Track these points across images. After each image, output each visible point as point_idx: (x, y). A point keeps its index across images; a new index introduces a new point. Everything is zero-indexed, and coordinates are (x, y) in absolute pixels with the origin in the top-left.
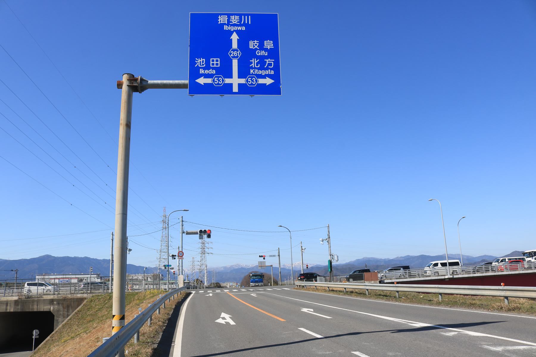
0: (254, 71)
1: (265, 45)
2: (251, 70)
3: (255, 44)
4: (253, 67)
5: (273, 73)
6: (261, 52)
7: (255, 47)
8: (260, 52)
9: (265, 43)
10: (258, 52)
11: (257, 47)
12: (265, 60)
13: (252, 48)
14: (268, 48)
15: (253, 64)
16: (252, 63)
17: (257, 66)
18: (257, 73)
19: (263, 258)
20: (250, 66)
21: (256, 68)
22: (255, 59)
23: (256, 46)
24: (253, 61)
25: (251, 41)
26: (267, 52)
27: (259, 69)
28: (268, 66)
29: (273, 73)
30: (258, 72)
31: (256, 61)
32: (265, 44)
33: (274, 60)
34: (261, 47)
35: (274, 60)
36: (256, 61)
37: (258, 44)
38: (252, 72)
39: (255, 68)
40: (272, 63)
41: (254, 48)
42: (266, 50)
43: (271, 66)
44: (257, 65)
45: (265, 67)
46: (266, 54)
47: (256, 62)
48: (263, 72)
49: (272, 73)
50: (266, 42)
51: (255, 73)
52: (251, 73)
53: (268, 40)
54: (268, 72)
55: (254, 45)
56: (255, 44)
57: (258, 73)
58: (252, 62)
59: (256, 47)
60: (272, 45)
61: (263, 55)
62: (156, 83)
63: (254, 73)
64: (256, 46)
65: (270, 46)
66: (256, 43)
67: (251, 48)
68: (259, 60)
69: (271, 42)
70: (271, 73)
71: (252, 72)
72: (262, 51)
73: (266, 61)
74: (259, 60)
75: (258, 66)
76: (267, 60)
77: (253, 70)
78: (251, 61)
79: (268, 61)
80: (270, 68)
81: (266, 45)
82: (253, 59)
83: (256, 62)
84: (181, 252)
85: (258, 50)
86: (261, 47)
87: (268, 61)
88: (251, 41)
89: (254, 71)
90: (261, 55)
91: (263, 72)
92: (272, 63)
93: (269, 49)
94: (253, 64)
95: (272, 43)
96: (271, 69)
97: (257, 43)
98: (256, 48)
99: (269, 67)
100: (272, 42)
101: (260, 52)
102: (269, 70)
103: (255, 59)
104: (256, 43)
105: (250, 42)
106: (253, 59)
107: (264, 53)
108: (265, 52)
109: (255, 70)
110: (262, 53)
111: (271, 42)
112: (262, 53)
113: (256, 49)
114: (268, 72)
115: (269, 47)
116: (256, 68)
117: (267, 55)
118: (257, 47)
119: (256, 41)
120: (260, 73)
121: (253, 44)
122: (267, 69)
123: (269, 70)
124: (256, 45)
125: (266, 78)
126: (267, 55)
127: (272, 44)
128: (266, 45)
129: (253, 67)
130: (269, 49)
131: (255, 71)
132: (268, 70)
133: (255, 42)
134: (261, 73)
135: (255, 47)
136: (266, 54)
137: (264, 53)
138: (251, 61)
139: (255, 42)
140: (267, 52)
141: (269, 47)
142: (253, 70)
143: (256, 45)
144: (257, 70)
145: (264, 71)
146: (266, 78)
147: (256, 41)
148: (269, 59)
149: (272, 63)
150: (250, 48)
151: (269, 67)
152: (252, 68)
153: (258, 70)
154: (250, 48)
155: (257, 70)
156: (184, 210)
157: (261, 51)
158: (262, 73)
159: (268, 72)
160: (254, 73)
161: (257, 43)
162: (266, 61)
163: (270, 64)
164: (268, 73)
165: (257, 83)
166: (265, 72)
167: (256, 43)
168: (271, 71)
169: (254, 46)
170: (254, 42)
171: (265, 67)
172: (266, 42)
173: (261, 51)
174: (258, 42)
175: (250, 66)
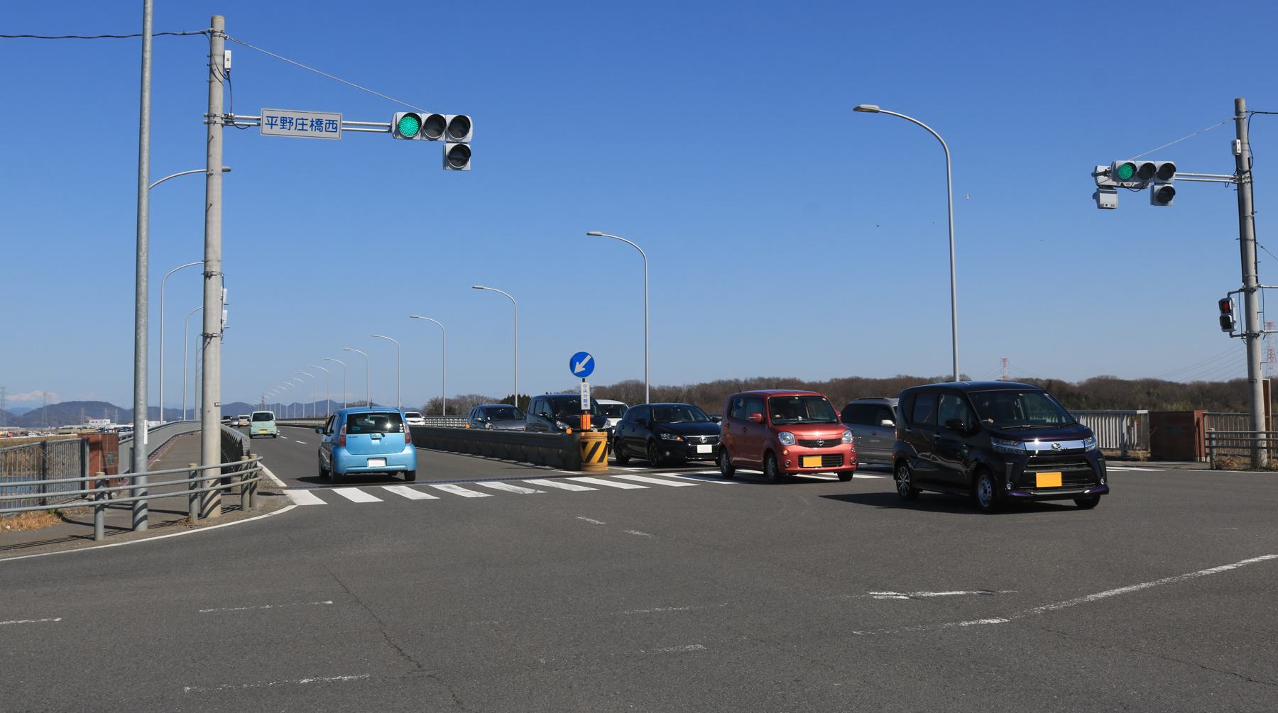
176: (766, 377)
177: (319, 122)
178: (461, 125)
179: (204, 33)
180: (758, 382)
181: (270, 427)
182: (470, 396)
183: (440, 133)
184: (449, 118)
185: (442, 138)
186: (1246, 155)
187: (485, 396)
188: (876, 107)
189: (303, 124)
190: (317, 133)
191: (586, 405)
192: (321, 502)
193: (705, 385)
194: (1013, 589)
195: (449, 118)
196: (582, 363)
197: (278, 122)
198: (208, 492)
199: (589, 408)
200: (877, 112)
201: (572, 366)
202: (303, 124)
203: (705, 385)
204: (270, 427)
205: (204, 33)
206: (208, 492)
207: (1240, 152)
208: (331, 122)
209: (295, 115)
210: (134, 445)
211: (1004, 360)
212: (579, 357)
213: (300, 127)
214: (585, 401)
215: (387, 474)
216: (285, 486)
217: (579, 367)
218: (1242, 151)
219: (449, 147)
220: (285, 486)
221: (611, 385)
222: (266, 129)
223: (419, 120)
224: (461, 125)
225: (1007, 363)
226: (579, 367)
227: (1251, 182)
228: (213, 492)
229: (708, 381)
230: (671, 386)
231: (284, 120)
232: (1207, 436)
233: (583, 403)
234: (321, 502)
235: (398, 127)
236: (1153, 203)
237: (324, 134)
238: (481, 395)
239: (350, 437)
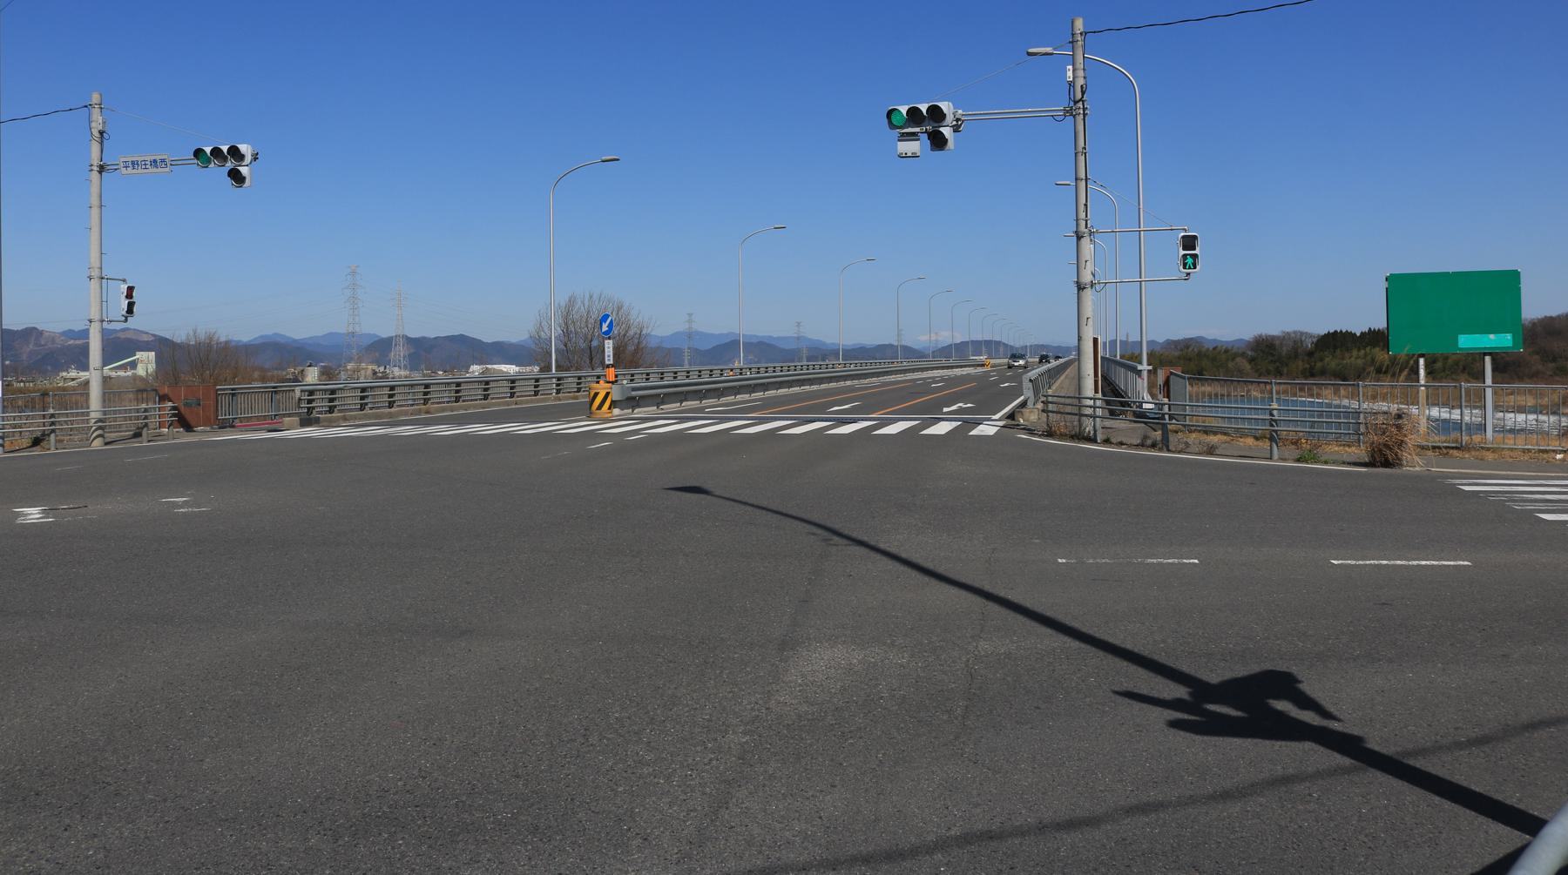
177: (155, 161)
179: (86, 106)
182: (1295, 332)
186: (1080, 82)
187: (1309, 332)
188: (1049, 50)
189: (145, 164)
190: (155, 170)
191: (609, 360)
192: (971, 433)
193: (1551, 318)
197: (130, 165)
198: (92, 427)
199: (612, 362)
200: (1052, 54)
202: (145, 164)
203: (1551, 317)
205: (86, 106)
206: (92, 427)
207: (1071, 79)
208: (163, 161)
209: (140, 159)
213: (144, 167)
214: (609, 356)
218: (1074, 78)
221: (1543, 316)
222: (124, 171)
228: (94, 428)
229: (1554, 312)
231: (133, 163)
233: (606, 358)
234: (971, 433)
236: (931, 150)
237: (160, 170)
238: (1306, 331)
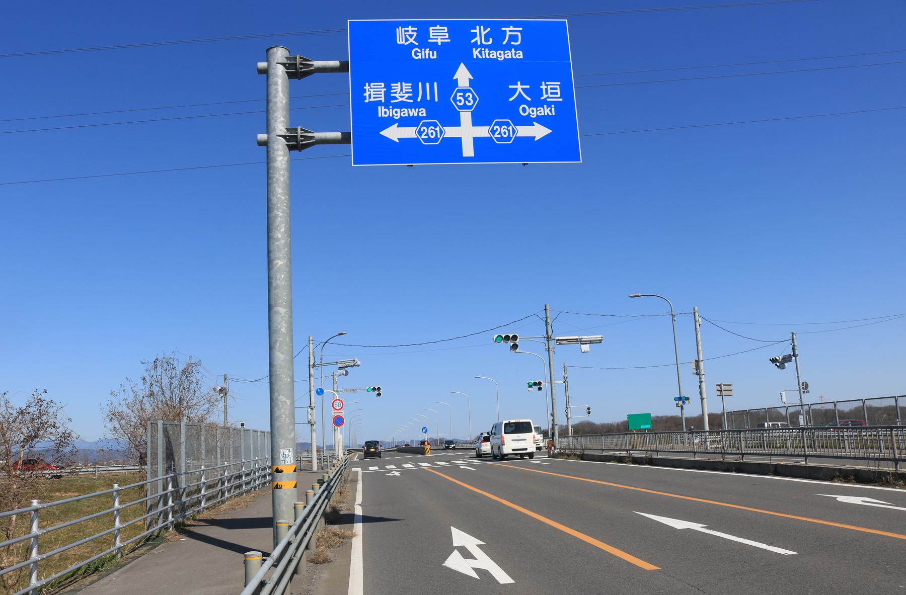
0: (480, 52)
1: (431, 37)
2: (474, 49)
3: (409, 35)
4: (479, 43)
5: (522, 57)
6: (423, 52)
7: (408, 40)
8: (419, 51)
9: (431, 31)
10: (416, 52)
11: (414, 40)
12: (503, 29)
13: (403, 42)
14: (438, 42)
15: (478, 38)
16: (476, 36)
17: (486, 41)
18: (488, 57)
19: (537, 387)
20: (472, 41)
21: (486, 47)
22: (482, 27)
23: (411, 38)
24: (477, 31)
25: (400, 27)
26: (435, 52)
27: (490, 48)
28: (509, 41)
29: (522, 57)
30: (489, 54)
31: (484, 30)
32: (431, 34)
33: (521, 29)
34: (423, 40)
35: (521, 29)
36: (484, 30)
37: (415, 34)
38: (476, 55)
39: (482, 46)
40: (517, 35)
41: (406, 44)
42: (433, 47)
43: (517, 41)
44: (487, 40)
45: (504, 43)
46: (433, 55)
47: (483, 33)
48: (500, 54)
49: (519, 56)
50: (433, 30)
51: (484, 57)
52: (475, 57)
53: (438, 26)
54: (510, 54)
55: (407, 36)
56: (409, 35)
57: (489, 56)
58: (476, 33)
59: (411, 40)
60: (447, 37)
61: (427, 57)
62: (320, 66)
63: (481, 55)
64: (411, 38)
65: (441, 39)
66: (410, 31)
67: (401, 43)
68: (489, 29)
69: (444, 30)
70: (517, 55)
71: (476, 55)
72: (425, 50)
73: (506, 31)
74: (489, 29)
75: (489, 41)
76: (507, 29)
77: (479, 49)
78: (472, 31)
79: (510, 31)
80: (514, 46)
81: (433, 36)
82: (477, 27)
83: (483, 33)
84: (338, 402)
85: (415, 46)
86: (423, 40)
87: (510, 31)
88: (400, 27)
89: (480, 52)
90: (424, 58)
91: (500, 54)
92: (519, 34)
93: (440, 44)
94: (478, 38)
95: (446, 31)
96: (517, 48)
97: (413, 31)
98: (411, 43)
99: (512, 43)
100: (446, 28)
101: (419, 51)
102: (513, 49)
103: (482, 27)
104: (410, 33)
105: (397, 29)
106: (477, 27)
107: (429, 54)
108: (431, 52)
109: (483, 49)
110: (425, 54)
111: (444, 30)
112: (425, 54)
113: (412, 46)
114: (512, 53)
115: (439, 41)
116: (486, 47)
117: (435, 57)
118: (414, 40)
119: (410, 27)
120: (493, 56)
121: (405, 35)
122: (508, 47)
123: (513, 49)
124: (411, 36)
125: (399, 139)
126: (435, 57)
127: (447, 34)
128: (433, 36)
129: (479, 43)
130: (440, 44)
131: (483, 52)
132: (511, 51)
133: (408, 31)
134: (495, 57)
135: (408, 40)
136: (433, 55)
137: (429, 54)
138: (472, 31)
139: (408, 31)
140: (435, 52)
141: (439, 41)
142: (479, 49)
143: (411, 36)
144: (487, 49)
145: (502, 52)
146: (399, 139)
147: (410, 27)
148: (511, 27)
149: (517, 35)
150: (398, 42)
151: (512, 43)
152: (475, 45)
153: (490, 50)
154: (398, 42)
155: (487, 49)
156: (339, 335)
157: (423, 50)
158: (497, 57)
159: (512, 53)
160: (480, 57)
161: (413, 31)
162: (506, 31)
163: (514, 38)
164: (510, 57)
165: (418, 127)
166: (504, 54)
167: (410, 31)
168: (517, 52)
169: (407, 40)
170: (406, 31)
171: (504, 43)
172: (433, 30)
173: (422, 51)
174: (416, 29)
175: (472, 41)
176: (660, 416)
178: (515, 337)
180: (656, 419)
181: (529, 442)
183: (508, 340)
184: (511, 336)
185: (510, 342)
194: (183, 529)
195: (511, 336)
196: (425, 430)
201: (423, 430)
204: (529, 442)
210: (457, 449)
211: (821, 397)
212: (424, 428)
215: (525, 457)
216: (395, 467)
217: (424, 431)
219: (512, 344)
220: (395, 467)
223: (502, 337)
224: (515, 337)
225: (823, 398)
226: (424, 431)
227: (309, 341)
230: (606, 423)
232: (333, 468)
235: (496, 339)
239: (804, 426)
